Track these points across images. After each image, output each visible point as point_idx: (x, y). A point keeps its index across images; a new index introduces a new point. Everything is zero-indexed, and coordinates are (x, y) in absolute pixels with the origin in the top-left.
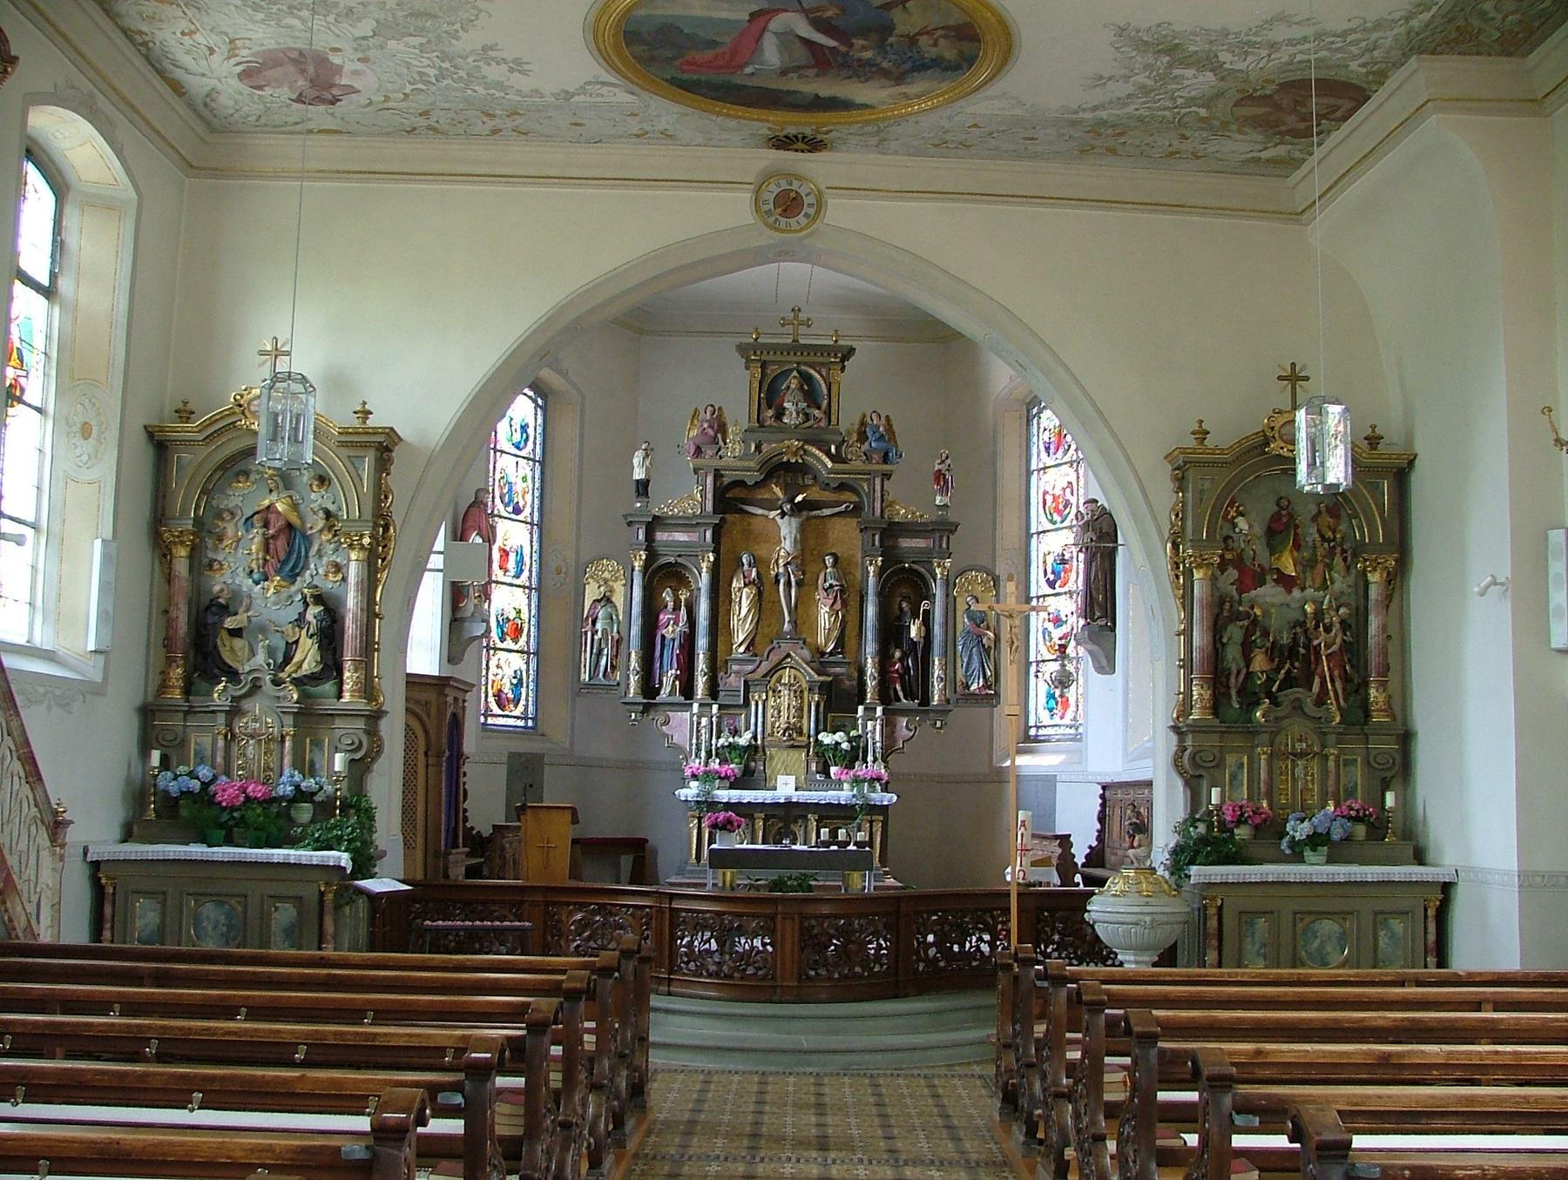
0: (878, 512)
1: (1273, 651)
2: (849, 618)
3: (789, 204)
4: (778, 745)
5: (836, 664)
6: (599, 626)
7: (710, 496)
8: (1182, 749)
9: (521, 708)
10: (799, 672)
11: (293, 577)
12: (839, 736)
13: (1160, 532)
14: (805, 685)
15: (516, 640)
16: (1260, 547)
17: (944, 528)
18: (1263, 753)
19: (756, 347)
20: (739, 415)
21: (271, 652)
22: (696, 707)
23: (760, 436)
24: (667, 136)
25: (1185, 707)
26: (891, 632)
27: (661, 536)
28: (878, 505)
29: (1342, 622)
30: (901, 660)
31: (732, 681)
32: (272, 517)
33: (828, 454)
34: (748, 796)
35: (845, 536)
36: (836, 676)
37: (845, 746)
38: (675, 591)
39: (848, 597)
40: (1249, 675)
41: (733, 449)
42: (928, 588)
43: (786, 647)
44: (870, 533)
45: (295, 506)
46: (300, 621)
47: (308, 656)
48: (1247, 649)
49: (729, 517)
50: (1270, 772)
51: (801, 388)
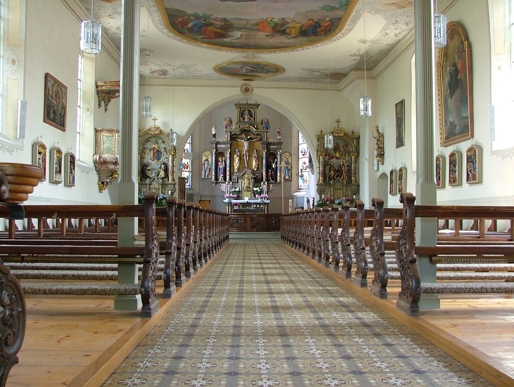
0: (265, 140)
1: (335, 171)
2: (260, 163)
3: (247, 90)
4: (245, 191)
5: (257, 173)
6: (206, 166)
7: (229, 137)
8: (318, 188)
9: (188, 184)
10: (249, 175)
11: (159, 160)
12: (258, 189)
13: (314, 149)
14: (250, 178)
15: (187, 169)
16: (333, 152)
17: (280, 144)
18: (332, 189)
19: (239, 104)
20: (235, 120)
21: (155, 173)
22: (227, 183)
23: (240, 124)
24: (225, 79)
25: (319, 181)
26: (269, 166)
27: (218, 146)
28: (265, 139)
29: (347, 165)
30: (271, 172)
31: (234, 177)
32: (155, 149)
33: (254, 127)
34: (238, 201)
35: (258, 145)
36: (257, 176)
37: (259, 191)
38: (222, 158)
39: (259, 159)
40: (330, 175)
41: (234, 127)
42: (276, 156)
43: (246, 170)
44: (264, 145)
45: (159, 147)
46: (160, 167)
47: (162, 174)
48: (330, 170)
49: (233, 141)
50: (333, 193)
51: (248, 113)
